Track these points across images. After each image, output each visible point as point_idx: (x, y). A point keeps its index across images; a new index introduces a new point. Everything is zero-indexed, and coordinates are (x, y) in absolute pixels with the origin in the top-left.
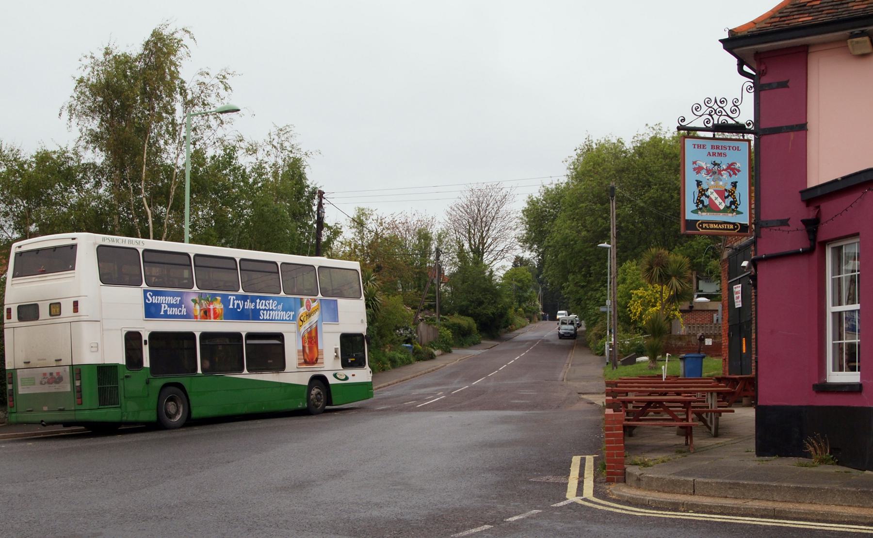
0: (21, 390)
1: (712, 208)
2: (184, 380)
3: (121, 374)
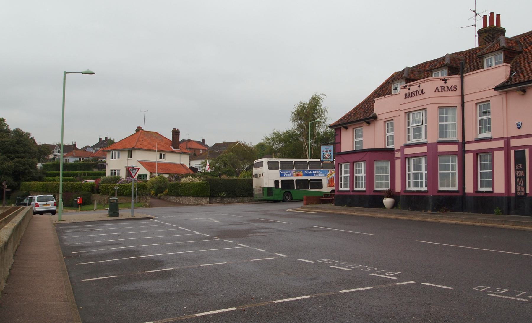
0: (255, 193)
1: (326, 158)
2: (291, 191)
3: (273, 189)
